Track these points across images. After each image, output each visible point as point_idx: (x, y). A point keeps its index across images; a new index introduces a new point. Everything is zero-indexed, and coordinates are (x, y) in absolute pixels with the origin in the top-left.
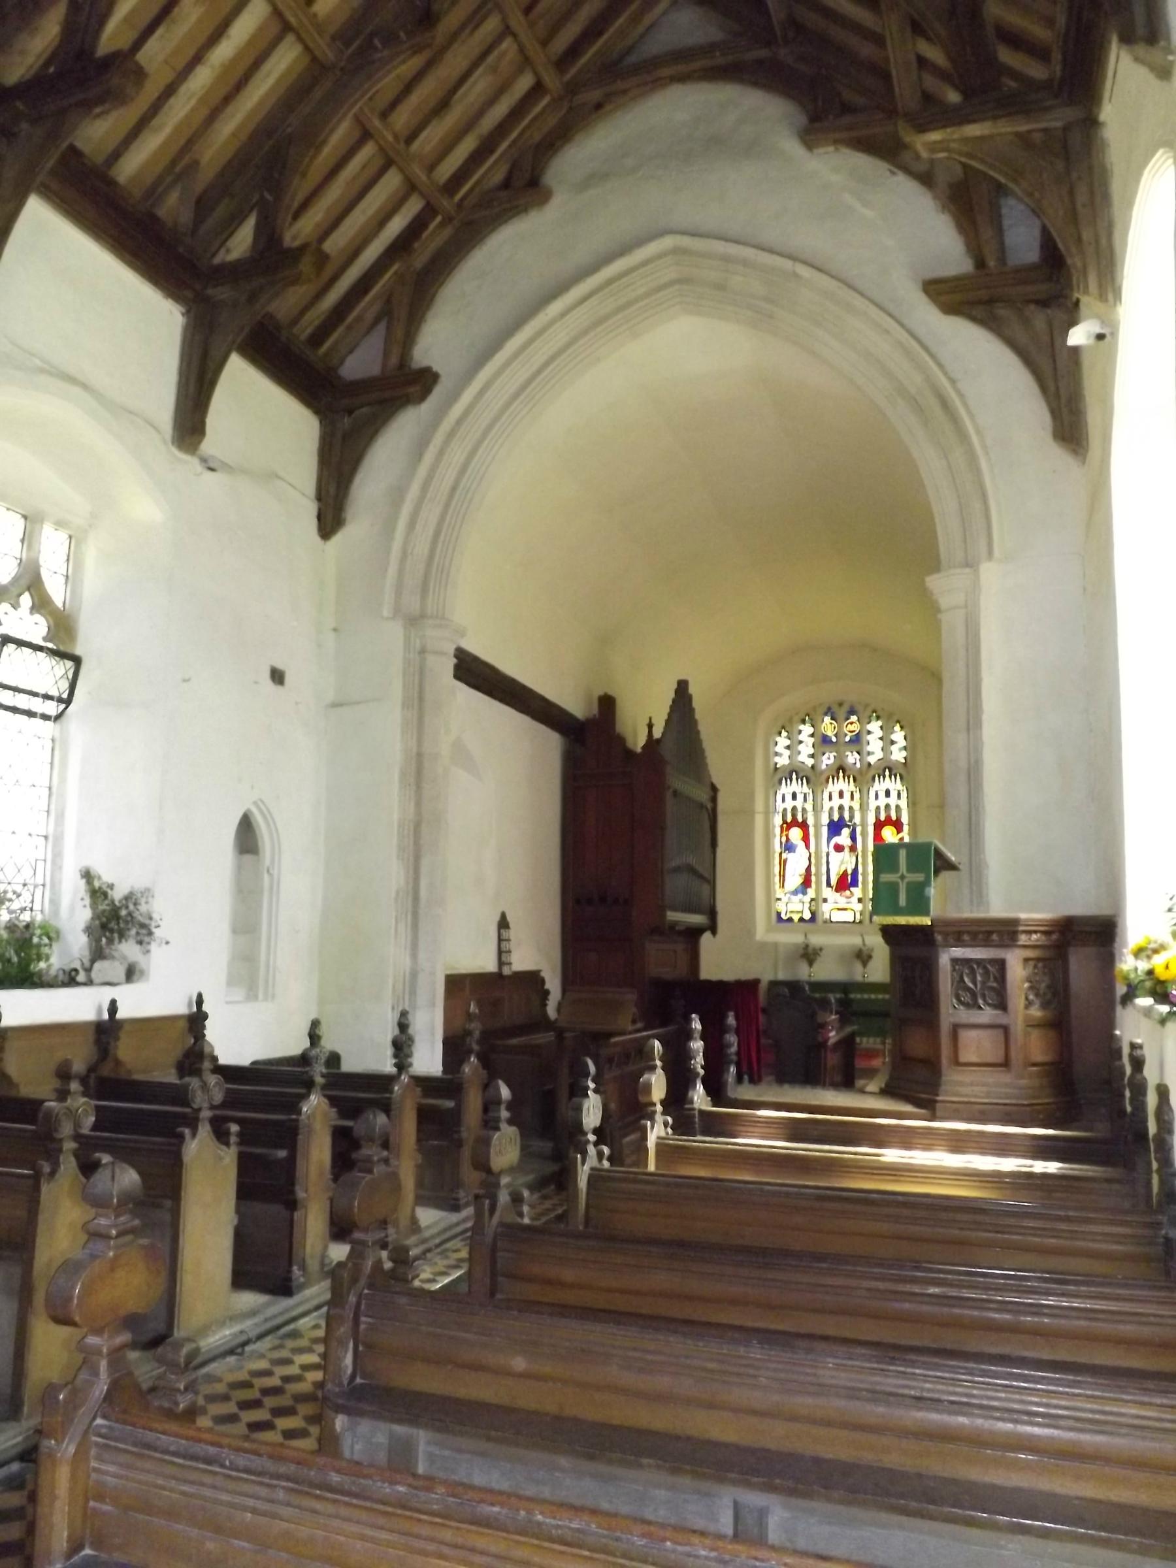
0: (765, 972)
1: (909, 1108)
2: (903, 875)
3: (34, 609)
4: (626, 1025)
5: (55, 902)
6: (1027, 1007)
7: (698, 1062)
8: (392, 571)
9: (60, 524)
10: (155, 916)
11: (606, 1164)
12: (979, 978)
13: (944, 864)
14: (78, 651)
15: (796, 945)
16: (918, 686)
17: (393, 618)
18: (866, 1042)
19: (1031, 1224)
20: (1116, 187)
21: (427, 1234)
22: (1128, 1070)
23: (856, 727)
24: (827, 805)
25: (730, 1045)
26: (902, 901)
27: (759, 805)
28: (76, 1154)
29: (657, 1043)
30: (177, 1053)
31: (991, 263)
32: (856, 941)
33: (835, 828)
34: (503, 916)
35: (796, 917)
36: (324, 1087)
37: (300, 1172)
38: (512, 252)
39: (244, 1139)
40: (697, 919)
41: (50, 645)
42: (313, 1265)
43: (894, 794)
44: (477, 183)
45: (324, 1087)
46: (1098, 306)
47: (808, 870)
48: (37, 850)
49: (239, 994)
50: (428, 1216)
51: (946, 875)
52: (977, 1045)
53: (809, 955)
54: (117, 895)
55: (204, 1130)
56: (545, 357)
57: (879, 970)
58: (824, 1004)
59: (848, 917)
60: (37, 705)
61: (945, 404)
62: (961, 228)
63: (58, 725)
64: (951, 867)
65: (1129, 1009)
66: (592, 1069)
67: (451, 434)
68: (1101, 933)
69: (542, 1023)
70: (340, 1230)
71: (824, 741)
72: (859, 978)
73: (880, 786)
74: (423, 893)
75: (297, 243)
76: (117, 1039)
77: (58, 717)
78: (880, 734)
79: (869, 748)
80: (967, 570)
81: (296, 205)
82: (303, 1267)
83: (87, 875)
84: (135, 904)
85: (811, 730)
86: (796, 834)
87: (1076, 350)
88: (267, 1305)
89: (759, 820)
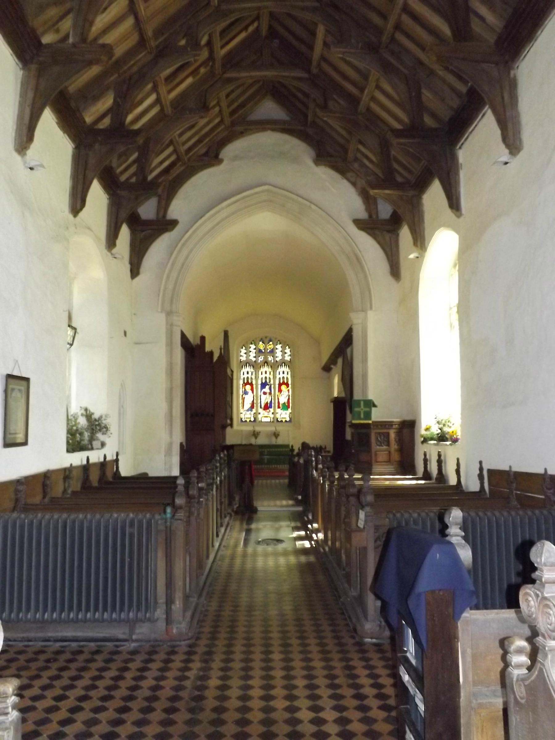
15: (250, 431)
17: (161, 312)
23: (272, 346)
24: (260, 376)
26: (362, 416)
31: (374, 217)
32: (273, 429)
33: (264, 385)
35: (248, 420)
43: (286, 373)
47: (253, 401)
52: (382, 456)
53: (255, 434)
59: (268, 420)
61: (358, 259)
67: (183, 245)
73: (281, 369)
79: (277, 355)
80: (364, 313)
86: (248, 387)
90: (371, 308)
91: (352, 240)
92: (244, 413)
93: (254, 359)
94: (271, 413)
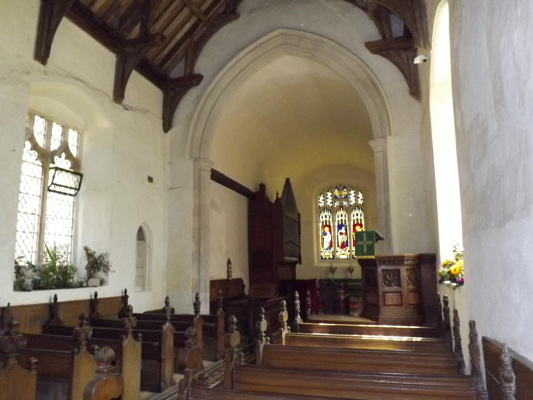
0: (317, 276)
1: (369, 321)
2: (365, 242)
3: (67, 158)
4: (272, 296)
5: (75, 259)
6: (408, 285)
7: (298, 307)
8: (189, 142)
9: (74, 129)
10: (110, 263)
11: (269, 343)
12: (392, 276)
13: (379, 238)
14: (82, 172)
15: (328, 267)
16: (367, 178)
18: (352, 299)
19: (412, 358)
20: (428, 10)
21: (206, 370)
22: (443, 305)
23: (346, 193)
25: (308, 302)
26: (365, 251)
27: (314, 220)
28: (86, 345)
29: (285, 302)
30: (118, 310)
31: (388, 37)
32: (348, 265)
33: (340, 227)
34: (229, 260)
35: (328, 258)
36: (171, 320)
37: (163, 349)
38: (226, 36)
39: (144, 339)
40: (294, 259)
41: (72, 170)
42: (168, 382)
44: (215, 11)
45: (171, 320)
46: (425, 51)
47: (331, 241)
48: (68, 241)
49: (139, 289)
50: (207, 364)
51: (379, 242)
52: (391, 299)
53: (332, 270)
54: (97, 255)
55: (130, 336)
56: (239, 70)
57: (357, 273)
58: (339, 287)
60: (68, 191)
61: (374, 84)
62: (377, 26)
63: (75, 198)
64: (381, 239)
65: (442, 285)
66: (263, 310)
68: (431, 259)
69: (243, 296)
70: (180, 368)
71: (335, 198)
72: (350, 277)
73: (354, 212)
74: (202, 253)
75: (154, 33)
76: (98, 305)
77: (75, 195)
78: (354, 195)
79: (351, 200)
81: (153, 20)
82: (165, 383)
83: (86, 249)
84: (103, 259)
85: (331, 194)
86: (327, 229)
87: (416, 65)
88: (152, 396)
89: (314, 225)
90: (390, 134)
91: (366, 65)
92: (324, 252)
93: (331, 205)
94: (347, 251)
